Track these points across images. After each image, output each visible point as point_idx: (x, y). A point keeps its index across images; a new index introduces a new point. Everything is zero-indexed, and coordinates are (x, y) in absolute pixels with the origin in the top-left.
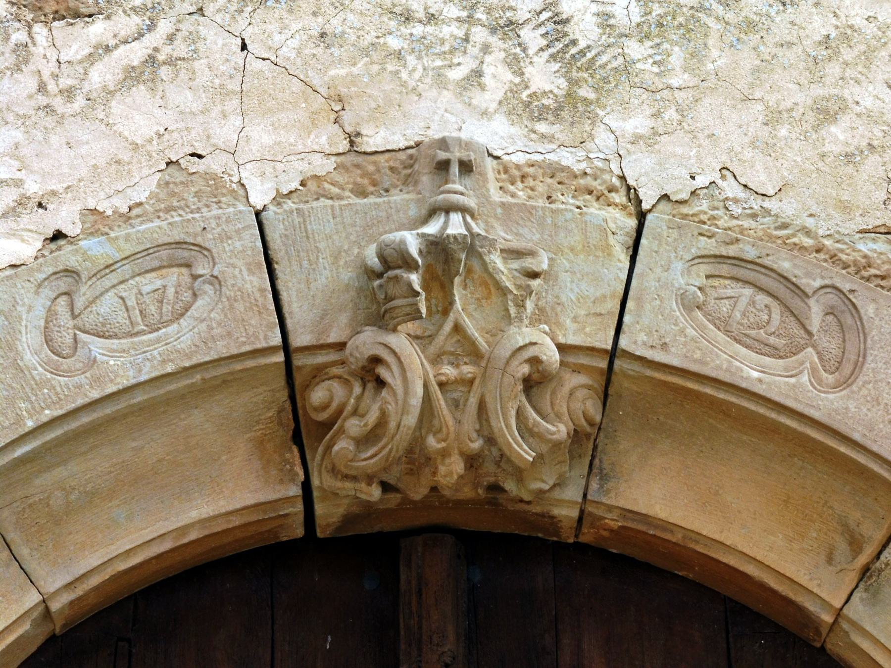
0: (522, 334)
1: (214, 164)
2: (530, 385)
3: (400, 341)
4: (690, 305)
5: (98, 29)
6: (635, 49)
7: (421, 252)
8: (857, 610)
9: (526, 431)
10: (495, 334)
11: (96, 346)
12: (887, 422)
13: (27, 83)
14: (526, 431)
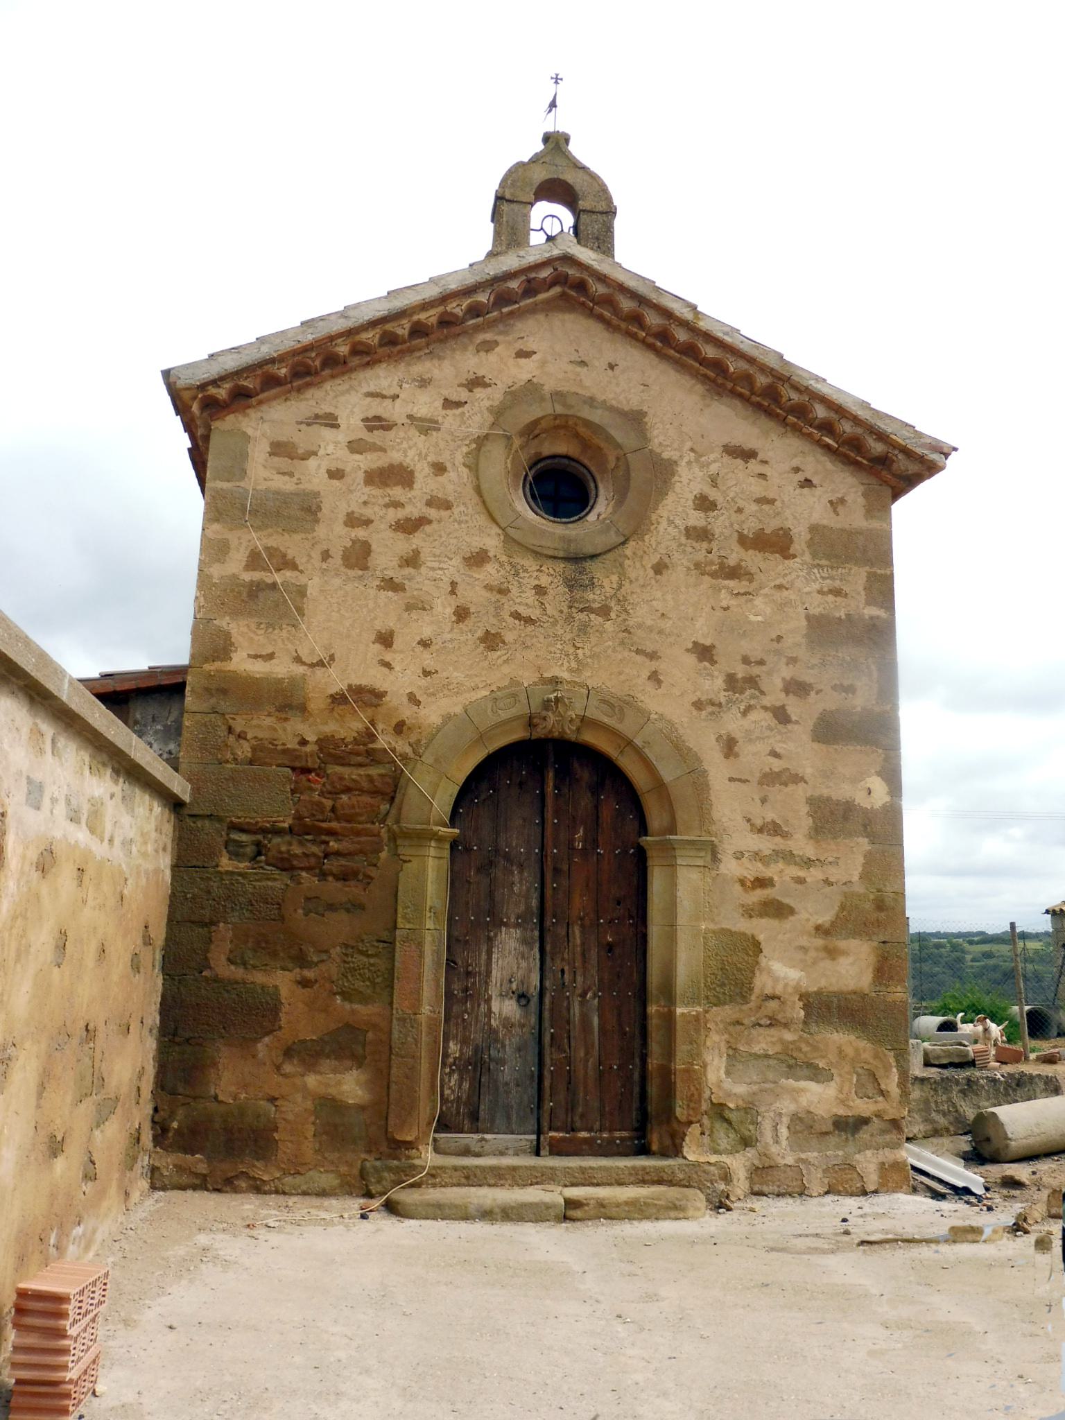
0: (570, 713)
1: (518, 679)
2: (570, 721)
3: (550, 713)
4: (597, 708)
5: (499, 653)
6: (589, 660)
7: (994, 1114)
8: (620, 758)
9: (569, 728)
10: (565, 712)
11: (500, 712)
12: (324, 566)
13: (487, 662)
14: (569, 728)
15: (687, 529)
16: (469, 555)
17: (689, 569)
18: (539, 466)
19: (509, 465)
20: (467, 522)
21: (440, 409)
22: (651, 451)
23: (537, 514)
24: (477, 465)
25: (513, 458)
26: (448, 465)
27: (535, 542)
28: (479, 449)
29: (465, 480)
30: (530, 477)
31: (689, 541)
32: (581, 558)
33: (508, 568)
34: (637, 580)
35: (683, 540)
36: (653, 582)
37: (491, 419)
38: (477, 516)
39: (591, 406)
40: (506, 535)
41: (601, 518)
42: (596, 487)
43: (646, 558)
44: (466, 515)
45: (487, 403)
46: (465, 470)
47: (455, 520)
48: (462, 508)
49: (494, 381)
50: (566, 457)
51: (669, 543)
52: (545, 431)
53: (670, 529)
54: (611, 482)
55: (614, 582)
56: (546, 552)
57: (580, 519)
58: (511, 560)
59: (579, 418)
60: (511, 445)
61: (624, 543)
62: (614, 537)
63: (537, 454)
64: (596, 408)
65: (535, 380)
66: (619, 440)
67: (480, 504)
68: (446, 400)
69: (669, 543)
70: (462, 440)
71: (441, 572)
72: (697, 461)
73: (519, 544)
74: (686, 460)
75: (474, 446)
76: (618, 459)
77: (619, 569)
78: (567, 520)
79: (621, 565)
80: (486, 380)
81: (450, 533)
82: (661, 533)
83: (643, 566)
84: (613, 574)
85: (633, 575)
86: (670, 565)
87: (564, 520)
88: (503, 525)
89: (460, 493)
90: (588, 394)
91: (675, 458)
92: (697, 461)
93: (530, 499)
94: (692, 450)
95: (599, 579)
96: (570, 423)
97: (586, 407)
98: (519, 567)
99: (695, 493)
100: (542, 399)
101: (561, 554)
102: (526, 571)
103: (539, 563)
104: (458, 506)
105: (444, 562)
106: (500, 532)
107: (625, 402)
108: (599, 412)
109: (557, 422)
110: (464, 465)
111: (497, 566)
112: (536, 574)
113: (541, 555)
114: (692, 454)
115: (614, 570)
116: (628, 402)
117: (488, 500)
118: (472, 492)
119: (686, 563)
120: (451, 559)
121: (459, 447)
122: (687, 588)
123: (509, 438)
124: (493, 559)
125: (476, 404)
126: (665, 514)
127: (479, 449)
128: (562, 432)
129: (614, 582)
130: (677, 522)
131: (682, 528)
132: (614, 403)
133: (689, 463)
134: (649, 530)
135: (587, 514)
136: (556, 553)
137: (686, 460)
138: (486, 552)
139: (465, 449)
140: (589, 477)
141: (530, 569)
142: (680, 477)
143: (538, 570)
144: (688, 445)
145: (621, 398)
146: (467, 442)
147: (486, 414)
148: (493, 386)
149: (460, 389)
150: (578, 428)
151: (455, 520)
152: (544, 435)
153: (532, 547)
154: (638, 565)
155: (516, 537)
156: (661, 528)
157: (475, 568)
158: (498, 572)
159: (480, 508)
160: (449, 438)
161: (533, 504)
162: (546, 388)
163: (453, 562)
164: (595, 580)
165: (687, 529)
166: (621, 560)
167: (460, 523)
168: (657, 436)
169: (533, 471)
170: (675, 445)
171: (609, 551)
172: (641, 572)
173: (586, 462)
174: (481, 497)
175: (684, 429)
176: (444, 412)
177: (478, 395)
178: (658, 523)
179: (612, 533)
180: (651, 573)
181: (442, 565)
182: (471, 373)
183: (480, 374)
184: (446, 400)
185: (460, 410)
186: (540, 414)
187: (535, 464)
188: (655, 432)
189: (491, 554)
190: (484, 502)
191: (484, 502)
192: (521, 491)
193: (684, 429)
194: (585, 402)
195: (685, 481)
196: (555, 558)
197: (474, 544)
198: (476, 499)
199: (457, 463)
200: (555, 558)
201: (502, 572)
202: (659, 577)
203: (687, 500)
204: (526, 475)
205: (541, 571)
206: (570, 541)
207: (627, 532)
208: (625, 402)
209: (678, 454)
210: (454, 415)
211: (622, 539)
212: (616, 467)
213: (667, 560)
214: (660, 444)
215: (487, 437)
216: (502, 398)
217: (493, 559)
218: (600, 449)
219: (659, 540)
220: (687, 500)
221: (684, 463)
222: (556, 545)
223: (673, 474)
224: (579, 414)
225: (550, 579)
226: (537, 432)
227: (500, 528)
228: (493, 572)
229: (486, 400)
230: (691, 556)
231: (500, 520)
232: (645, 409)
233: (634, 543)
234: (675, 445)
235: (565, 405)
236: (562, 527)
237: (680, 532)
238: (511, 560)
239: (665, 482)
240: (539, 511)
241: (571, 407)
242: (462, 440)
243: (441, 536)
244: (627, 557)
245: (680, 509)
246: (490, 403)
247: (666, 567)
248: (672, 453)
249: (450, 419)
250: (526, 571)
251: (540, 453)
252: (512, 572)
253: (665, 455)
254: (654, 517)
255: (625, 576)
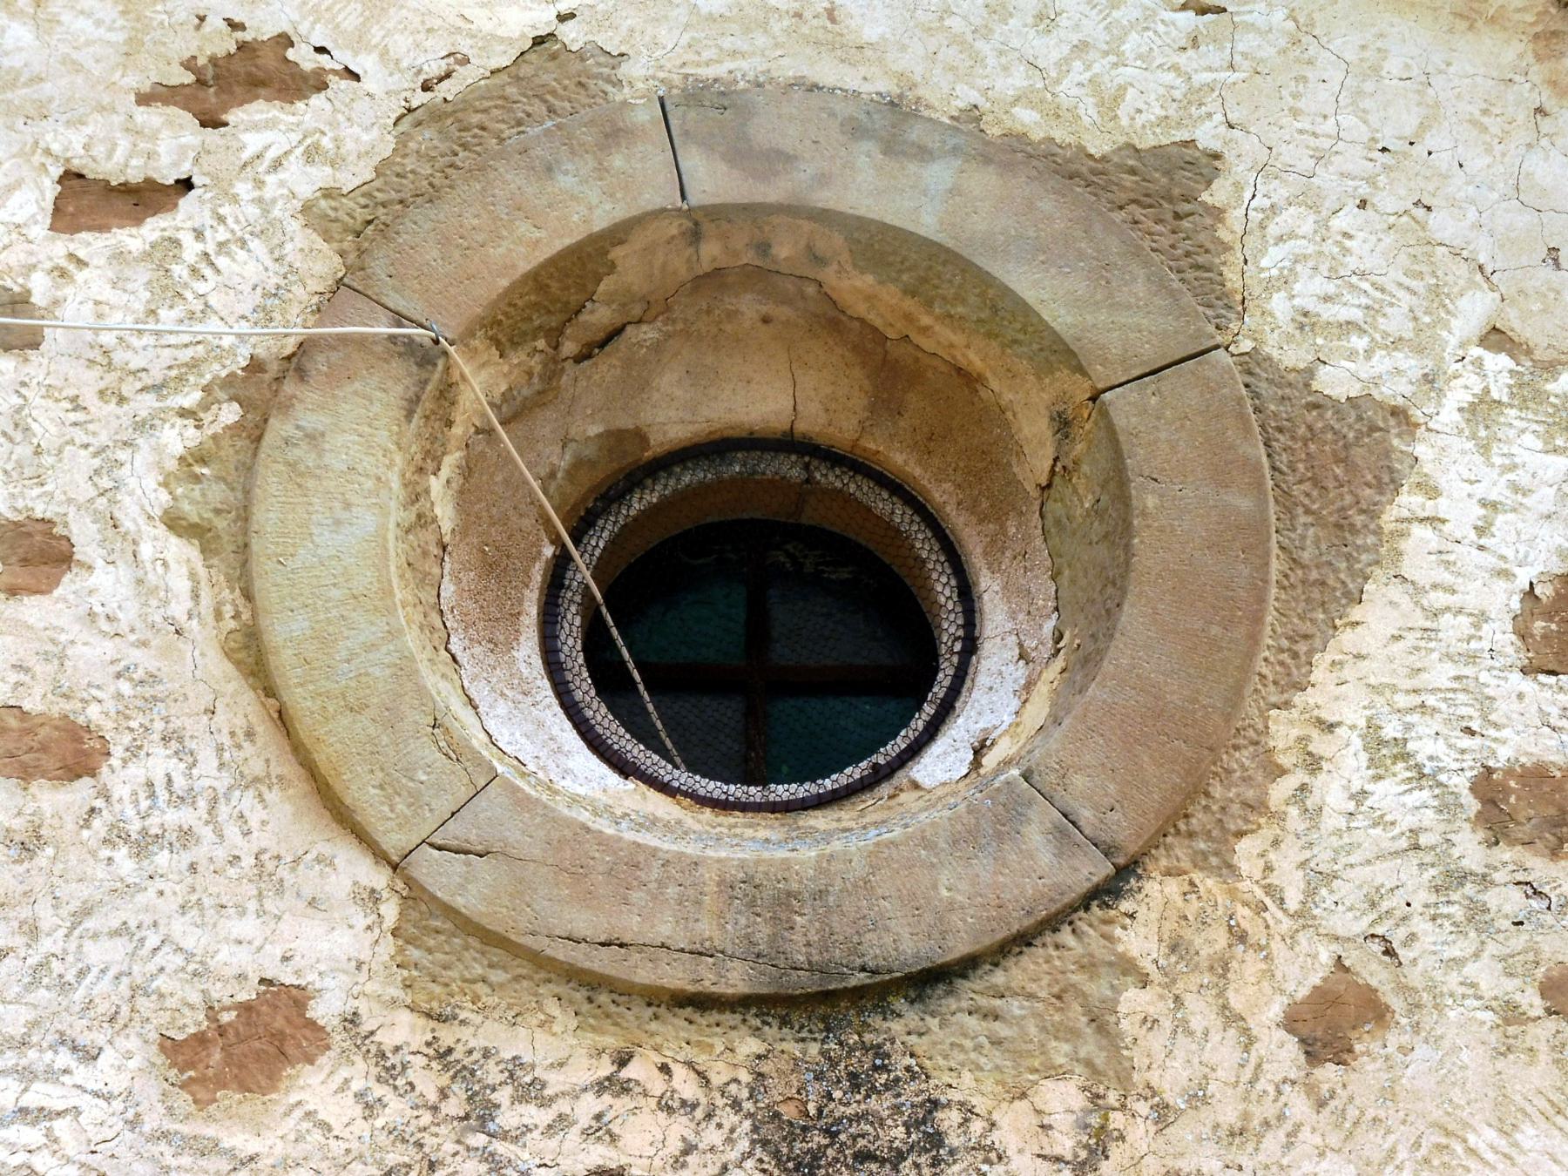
15: (1488, 786)
16: (194, 1022)
17: (1511, 1014)
18: (638, 503)
19: (445, 514)
20: (187, 835)
21: (40, 230)
22: (1252, 363)
23: (623, 767)
24: (244, 515)
25: (467, 470)
26: (84, 534)
27: (584, 922)
28: (253, 432)
29: (179, 609)
30: (583, 572)
31: (1505, 853)
32: (858, 993)
33: (428, 1083)
34: (1198, 1098)
35: (1470, 849)
36: (1299, 1106)
37: (323, 264)
38: (247, 801)
39: (893, 147)
40: (415, 895)
41: (990, 761)
42: (967, 595)
43: (1248, 966)
44: (184, 799)
45: (305, 180)
46: (180, 551)
47: (117, 835)
48: (160, 763)
49: (342, 57)
50: (788, 444)
51: (1383, 873)
52: (653, 308)
53: (1387, 793)
54: (1042, 557)
55: (1062, 1122)
56: (644, 973)
57: (880, 776)
58: (447, 1036)
59: (824, 217)
60: (447, 392)
61: (1106, 892)
62: (1045, 857)
63: (616, 438)
64: (924, 154)
65: (571, 34)
66: (1060, 316)
67: (264, 729)
68: (72, 178)
69: (1383, 873)
70: (158, 388)
71: (31, 1135)
72: (1527, 394)
73: (490, 939)
74: (1458, 396)
75: (230, 413)
76: (1063, 425)
77: (1090, 1047)
78: (801, 790)
79: (1101, 1021)
80: (301, 55)
81: (87, 911)
82: (1331, 821)
83: (1230, 1017)
84: (1055, 1073)
85: (1172, 1080)
86: (1396, 1003)
87: (781, 792)
88: (394, 841)
89: (153, 678)
90: (885, 85)
91: (1394, 390)
92: (1527, 394)
93: (583, 687)
94: (1496, 337)
95: (968, 1111)
96: (783, 251)
97: (866, 155)
98: (493, 1074)
99: (1523, 578)
100: (614, 133)
101: (737, 979)
102: (531, 1092)
103: (611, 1041)
104: (134, 751)
105: (53, 1075)
106: (379, 878)
107: (1089, 110)
108: (939, 174)
109: (711, 252)
110: (174, 523)
111: (360, 1074)
112: (589, 1105)
113: (622, 991)
114: (1498, 363)
115: (1060, 1052)
116: (1110, 104)
117: (300, 700)
118: (217, 667)
119: (1487, 976)
120: (90, 1056)
121: (143, 425)
122: (1506, 1130)
123: (425, 356)
124: (338, 1039)
125: (243, 189)
126: (1352, 713)
127: (253, 432)
128: (749, 306)
129: (1062, 1121)
130: (1424, 748)
131: (1460, 783)
132: (1027, 118)
133: (1481, 410)
134: (1258, 806)
135: (915, 750)
136: (709, 979)
137: (1458, 396)
138: (296, 998)
139: (176, 439)
140: (924, 545)
141: (556, 1082)
142: (1433, 492)
143: (602, 1087)
144: (1474, 309)
145: (1068, 89)
146: (191, 399)
147: (299, 238)
148: (338, 85)
149: (144, 116)
150: (829, 275)
151: (117, 835)
152: (648, 333)
153: (562, 952)
154: (1201, 1013)
155: (469, 902)
156: (1331, 793)
157: (230, 1097)
158: (370, 1108)
159: (264, 754)
160: (88, 382)
161: (599, 714)
162: (634, 70)
163: (107, 1072)
164: (949, 1119)
165: (1488, 786)
166: (1098, 989)
167: (143, 845)
168: (1283, 282)
169: (599, 540)
170: (1395, 322)
171: (1023, 940)
172: (1223, 1052)
173: (901, 460)
174: (270, 692)
175: (1443, 225)
176: (60, 247)
177: (253, 142)
178: (1314, 764)
179: (1036, 834)
180: (1284, 1054)
181: (39, 1096)
182: (215, 23)
183: (262, 27)
184: (72, 178)
185: (154, 228)
186: (604, 215)
187: (610, 496)
188: (1273, 259)
189: (325, 1010)
190: (283, 720)
191: (283, 720)
192: (528, 650)
193: (1443, 225)
194: (855, 130)
195: (1460, 512)
196: (701, 1002)
197: (229, 958)
198: (242, 706)
199: (130, 517)
200: (701, 1002)
201: (396, 1109)
202: (1328, 1074)
203: (1481, 618)
204: (562, 562)
205: (625, 1088)
206: (786, 900)
207: (1125, 831)
208: (1089, 110)
209: (1412, 365)
210: (119, 256)
211: (1094, 869)
212: (1061, 471)
213: (1373, 972)
214: (1305, 321)
215: (297, 362)
216: (387, 148)
217: (338, 1039)
218: (969, 379)
219: (1322, 858)
220: (1481, 618)
221: (1448, 414)
222: (706, 928)
223: (1389, 483)
224: (825, 198)
225: (680, 1127)
226: (599, 316)
227: (379, 855)
228: (339, 1111)
229: (294, 164)
230: (1519, 940)
231: (362, 793)
232: (1207, 136)
233: (1173, 887)
234: (1395, 322)
235: (741, 154)
236: (767, 829)
237: (1447, 806)
238: (447, 1036)
239: (1343, 526)
240: (636, 751)
241: (777, 160)
242: (158, 388)
243: (32, 931)
244: (1127, 967)
245: (1441, 674)
246: (321, 175)
247: (1375, 1011)
248: (1381, 363)
249: (94, 282)
250: (531, 1092)
251: (640, 436)
252: (454, 1106)
253: (1336, 381)
254: (1283, 731)
255: (1124, 1079)
